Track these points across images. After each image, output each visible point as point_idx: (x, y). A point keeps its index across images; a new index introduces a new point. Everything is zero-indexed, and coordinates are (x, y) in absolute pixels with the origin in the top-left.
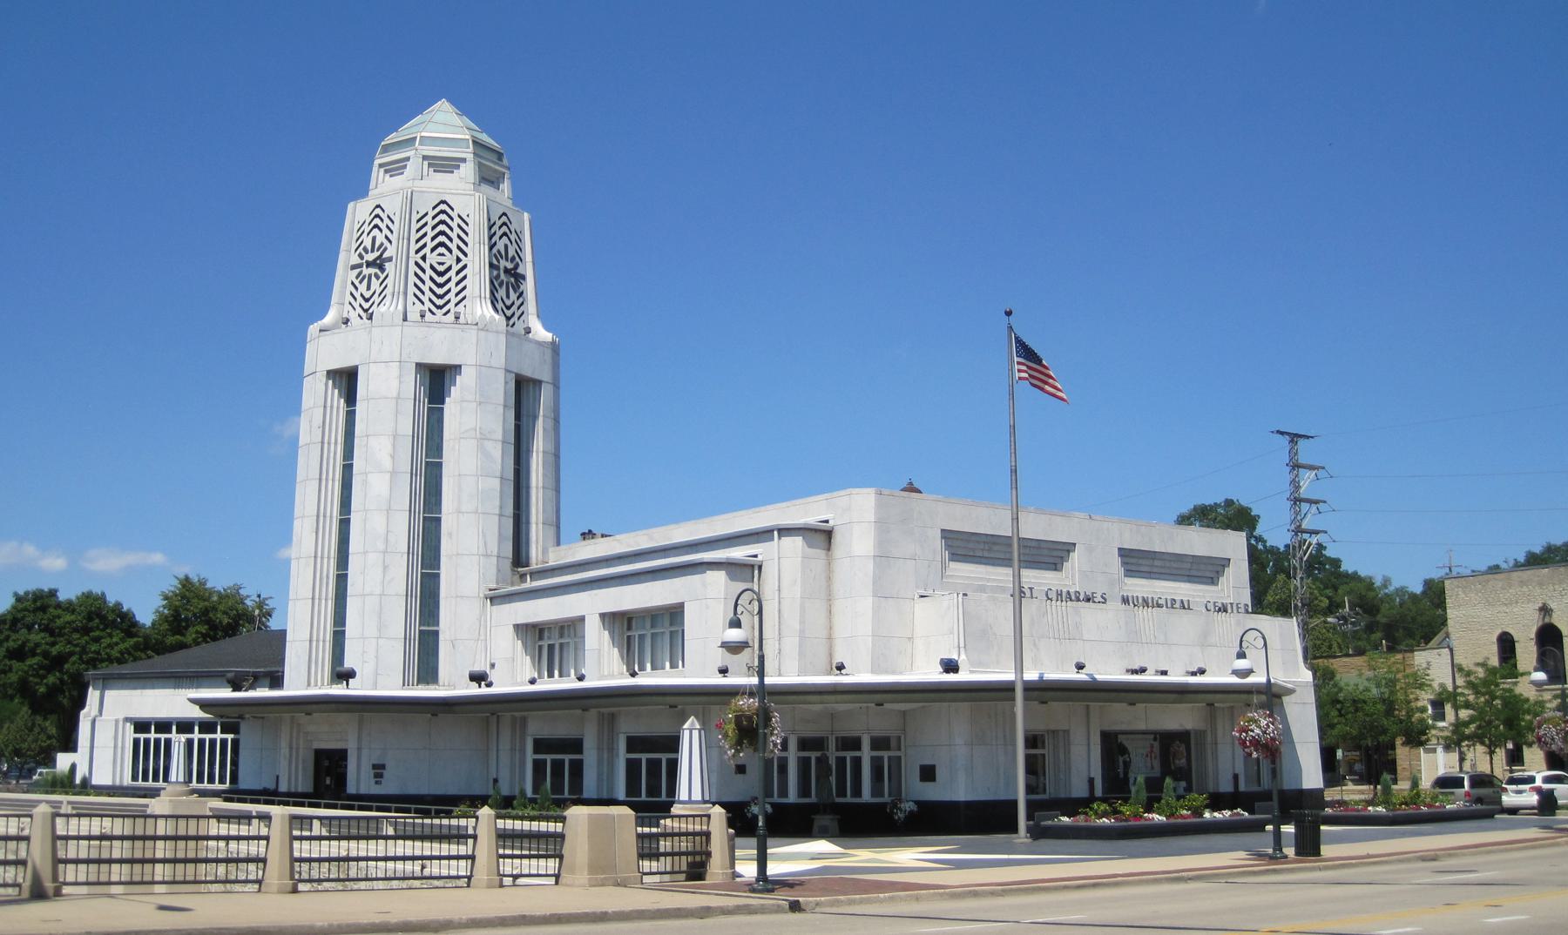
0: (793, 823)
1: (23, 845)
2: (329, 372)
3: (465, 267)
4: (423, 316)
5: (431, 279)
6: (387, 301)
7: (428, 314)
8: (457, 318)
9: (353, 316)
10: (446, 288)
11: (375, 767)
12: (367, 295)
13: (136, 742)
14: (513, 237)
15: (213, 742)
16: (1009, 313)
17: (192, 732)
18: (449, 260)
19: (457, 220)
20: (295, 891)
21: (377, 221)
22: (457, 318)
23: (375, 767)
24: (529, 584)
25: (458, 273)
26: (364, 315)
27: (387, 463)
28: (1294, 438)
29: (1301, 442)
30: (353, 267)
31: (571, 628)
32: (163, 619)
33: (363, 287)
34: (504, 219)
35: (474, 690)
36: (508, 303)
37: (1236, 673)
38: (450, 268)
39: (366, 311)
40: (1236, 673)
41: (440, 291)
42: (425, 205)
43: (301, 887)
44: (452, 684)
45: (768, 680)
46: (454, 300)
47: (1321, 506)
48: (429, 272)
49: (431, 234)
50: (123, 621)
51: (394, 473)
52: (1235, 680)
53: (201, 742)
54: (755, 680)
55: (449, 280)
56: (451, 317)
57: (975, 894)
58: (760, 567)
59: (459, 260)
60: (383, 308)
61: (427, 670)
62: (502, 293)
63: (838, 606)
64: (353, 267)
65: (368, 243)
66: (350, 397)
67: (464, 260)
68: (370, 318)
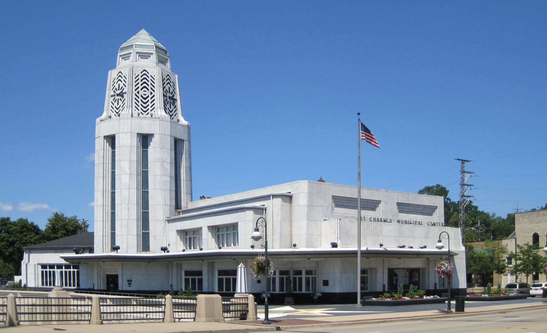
0: (277, 300)
1: (5, 308)
2: (104, 137)
3: (154, 96)
4: (139, 115)
5: (141, 105)
6: (125, 109)
7: (141, 114)
8: (152, 116)
9: (113, 115)
10: (147, 108)
11: (128, 281)
12: (118, 107)
13: (42, 272)
14: (172, 84)
15: (70, 272)
16: (359, 114)
17: (62, 268)
18: (148, 93)
19: (150, 78)
20: (102, 323)
21: (120, 78)
22: (152, 116)
23: (128, 281)
24: (181, 216)
25: (151, 98)
26: (117, 115)
27: (128, 171)
28: (463, 161)
29: (466, 163)
30: (112, 96)
31: (197, 231)
32: (49, 228)
33: (116, 104)
34: (168, 77)
35: (163, 254)
36: (171, 110)
37: (437, 247)
38: (148, 96)
39: (117, 113)
40: (437, 247)
41: (145, 105)
42: (138, 72)
43: (104, 322)
44: (155, 251)
45: (268, 250)
46: (150, 109)
47: (472, 187)
48: (141, 98)
49: (141, 83)
50: (35, 229)
51: (130, 175)
52: (437, 250)
53: (50, 272)
54: (264, 250)
55: (148, 105)
56: (149, 115)
57: (342, 325)
58: (266, 209)
59: (151, 93)
60: (123, 112)
61: (146, 247)
62: (168, 106)
63: (294, 223)
64: (112, 96)
65: (117, 87)
66: (113, 146)
67: (154, 93)
68: (119, 116)
